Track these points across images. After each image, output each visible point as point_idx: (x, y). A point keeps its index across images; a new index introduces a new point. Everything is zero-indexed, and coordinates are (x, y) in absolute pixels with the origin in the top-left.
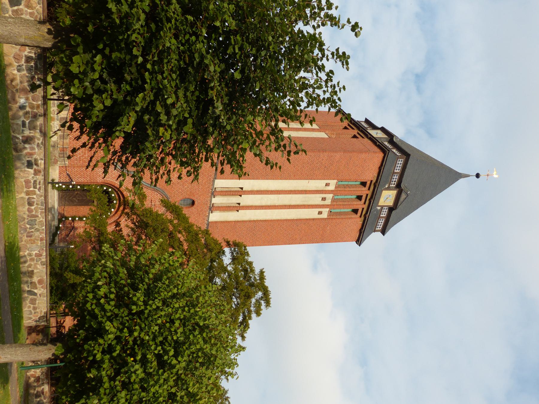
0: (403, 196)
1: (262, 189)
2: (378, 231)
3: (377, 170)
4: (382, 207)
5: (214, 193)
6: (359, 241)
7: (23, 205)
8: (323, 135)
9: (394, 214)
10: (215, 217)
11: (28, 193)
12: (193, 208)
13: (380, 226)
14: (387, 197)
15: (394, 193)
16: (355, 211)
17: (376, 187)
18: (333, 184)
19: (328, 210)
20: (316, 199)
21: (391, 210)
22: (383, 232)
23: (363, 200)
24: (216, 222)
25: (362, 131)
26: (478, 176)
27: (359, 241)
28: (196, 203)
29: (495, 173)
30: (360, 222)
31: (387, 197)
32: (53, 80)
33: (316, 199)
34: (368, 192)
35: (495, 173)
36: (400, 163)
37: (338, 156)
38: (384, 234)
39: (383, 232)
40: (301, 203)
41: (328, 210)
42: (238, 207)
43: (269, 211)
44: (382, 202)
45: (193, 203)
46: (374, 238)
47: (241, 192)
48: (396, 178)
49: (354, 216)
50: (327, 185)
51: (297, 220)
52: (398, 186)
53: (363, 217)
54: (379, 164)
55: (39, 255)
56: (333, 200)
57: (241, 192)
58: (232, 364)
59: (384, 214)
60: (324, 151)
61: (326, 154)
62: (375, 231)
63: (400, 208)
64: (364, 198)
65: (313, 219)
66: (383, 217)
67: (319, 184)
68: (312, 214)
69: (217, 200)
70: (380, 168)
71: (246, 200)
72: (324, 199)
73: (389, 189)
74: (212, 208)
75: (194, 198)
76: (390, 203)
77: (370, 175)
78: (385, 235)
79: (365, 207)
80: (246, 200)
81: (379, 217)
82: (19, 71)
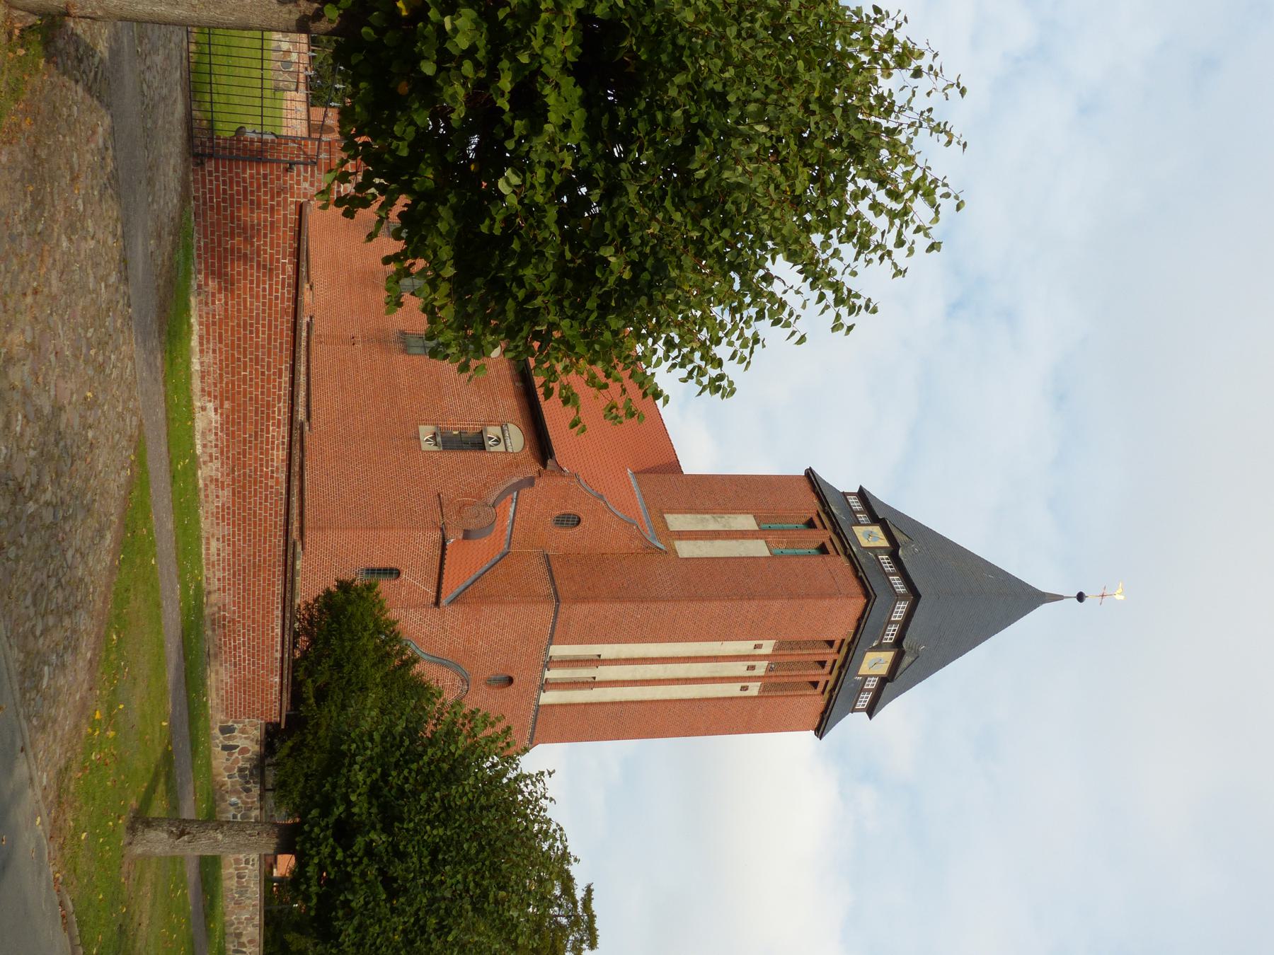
0: (907, 660)
1: (636, 656)
3: (854, 623)
4: (866, 677)
5: (550, 663)
6: (820, 731)
7: (231, 878)
8: (758, 548)
10: (548, 698)
11: (236, 869)
12: (511, 689)
13: (864, 700)
14: (875, 663)
15: (887, 656)
16: (815, 684)
17: (851, 650)
18: (768, 647)
19: (765, 663)
20: (739, 669)
21: (884, 681)
23: (828, 668)
24: (552, 706)
25: (838, 535)
26: (1081, 597)
27: (820, 731)
28: (516, 681)
29: (1120, 590)
30: (821, 702)
31: (875, 663)
33: (739, 669)
34: (836, 657)
35: (1120, 590)
36: (901, 609)
37: (776, 605)
38: (871, 716)
39: (871, 711)
40: (709, 675)
41: (765, 663)
42: (592, 684)
43: (648, 676)
44: (864, 669)
45: (510, 681)
46: (852, 725)
47: (597, 661)
48: (892, 631)
49: (811, 692)
50: (756, 647)
51: (699, 700)
52: (898, 643)
53: (826, 695)
54: (858, 615)
55: (250, 919)
56: (769, 669)
57: (597, 661)
59: (871, 684)
60: (751, 597)
61: (754, 604)
63: (900, 679)
65: (731, 698)
66: (869, 690)
67: (746, 647)
68: (733, 690)
69: (552, 674)
70: (860, 620)
72: (744, 688)
73: (880, 648)
74: (546, 685)
75: (511, 675)
76: (883, 670)
77: (842, 629)
79: (832, 679)
80: (237, 71)
81: (862, 690)
82: (230, 777)
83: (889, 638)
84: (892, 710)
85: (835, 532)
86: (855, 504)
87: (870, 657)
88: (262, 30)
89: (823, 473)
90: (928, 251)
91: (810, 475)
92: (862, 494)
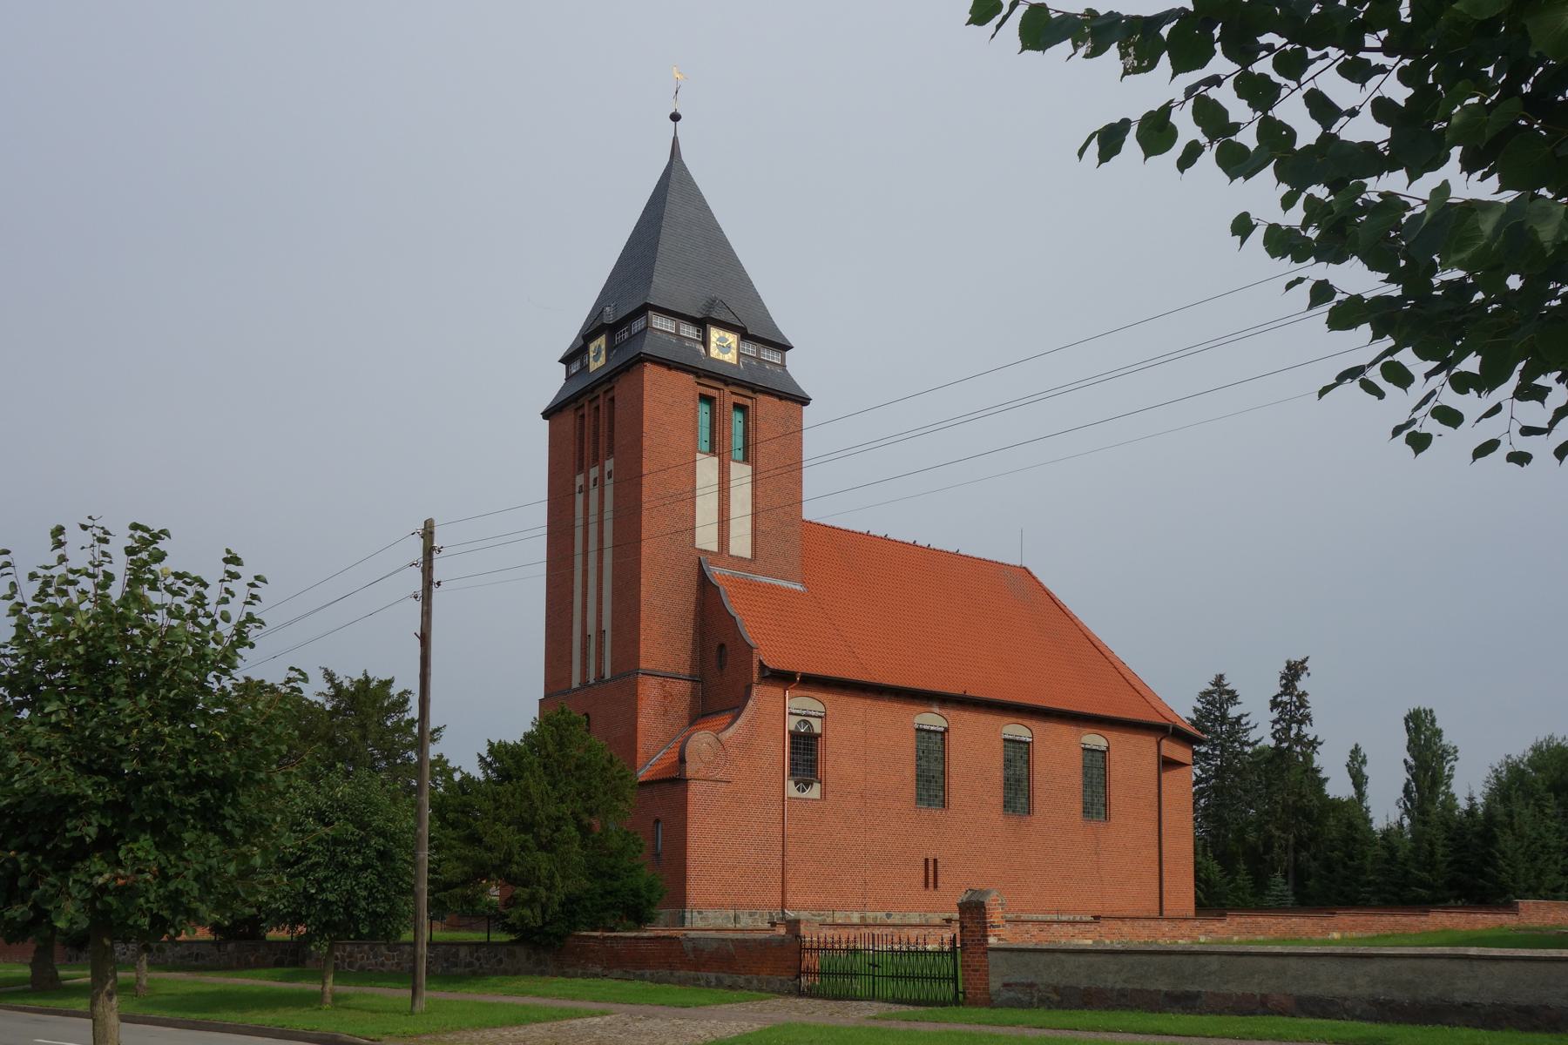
2: (783, 359)
4: (740, 355)
6: (805, 401)
9: (763, 337)
13: (775, 357)
15: (715, 334)
17: (711, 375)
21: (745, 336)
22: (784, 347)
26: (675, 117)
31: (723, 347)
32: (1207, 97)
39: (784, 347)
44: (730, 357)
46: (800, 368)
58: (1534, 749)
59: (750, 349)
62: (783, 366)
64: (741, 400)
66: (758, 352)
71: (592, 630)
73: (705, 343)
76: (732, 338)
78: (792, 341)
80: (592, 630)
83: (689, 331)
84: (786, 324)
85: (727, 385)
86: (575, 368)
87: (714, 352)
88: (735, 907)
89: (546, 400)
90: (1356, 752)
91: (546, 415)
92: (567, 360)
